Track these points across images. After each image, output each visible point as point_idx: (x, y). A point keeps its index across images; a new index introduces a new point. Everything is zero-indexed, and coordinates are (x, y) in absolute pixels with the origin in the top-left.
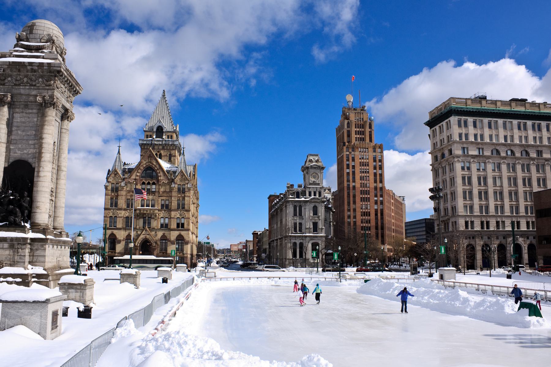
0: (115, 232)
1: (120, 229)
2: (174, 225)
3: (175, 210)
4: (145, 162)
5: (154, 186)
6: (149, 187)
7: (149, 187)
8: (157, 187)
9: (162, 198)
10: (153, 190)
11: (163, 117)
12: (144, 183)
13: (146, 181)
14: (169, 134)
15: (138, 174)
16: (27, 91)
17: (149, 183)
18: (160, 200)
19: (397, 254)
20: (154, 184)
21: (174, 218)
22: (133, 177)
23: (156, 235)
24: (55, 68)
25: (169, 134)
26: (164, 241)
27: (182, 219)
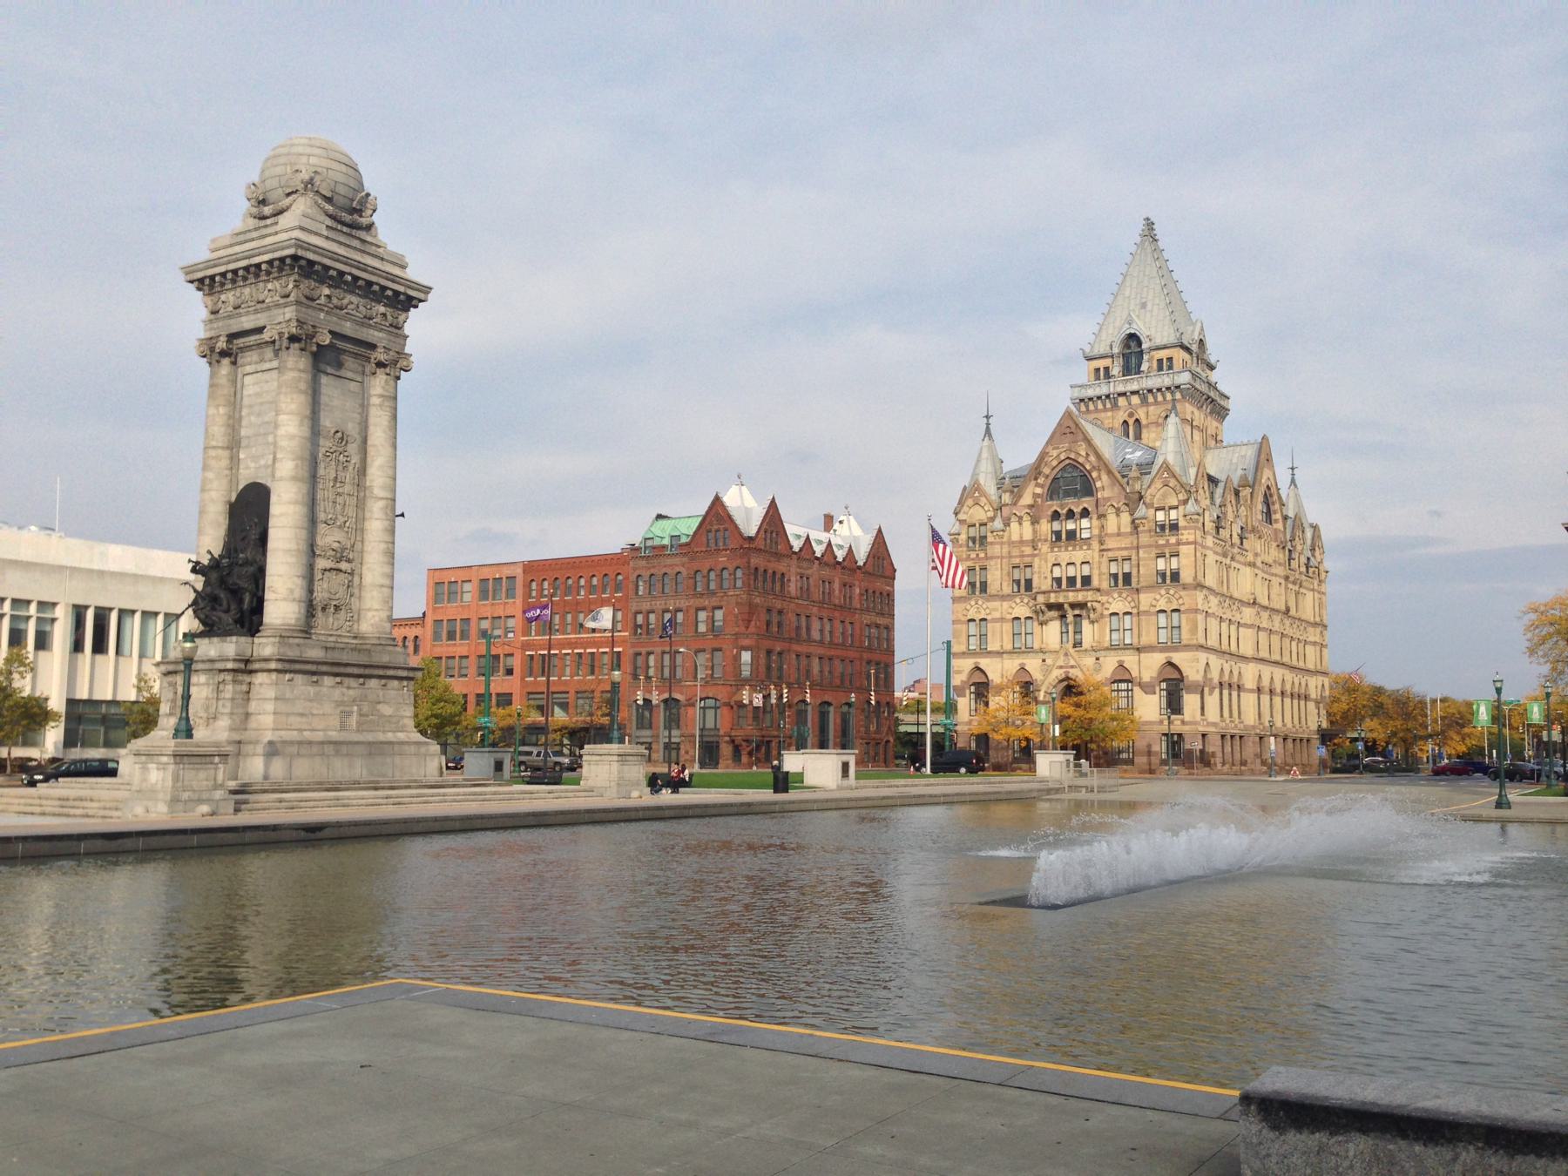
0: (984, 663)
1: (1000, 654)
2: (90, 952)
3: (1150, 588)
4: (1055, 453)
5: (1085, 523)
6: (1071, 526)
7: (1071, 526)
8: (1096, 522)
9: (1110, 554)
10: (1085, 535)
11: (1144, 306)
12: (1056, 516)
13: (1062, 507)
14: (1163, 354)
15: (1039, 490)
16: (252, 317)
17: (1070, 515)
18: (1105, 560)
19: (1407, 744)
20: (1085, 513)
21: (1147, 613)
22: (1027, 499)
23: (1098, 669)
24: (375, 526)
25: (1163, 354)
26: (1123, 686)
27: (1175, 615)
